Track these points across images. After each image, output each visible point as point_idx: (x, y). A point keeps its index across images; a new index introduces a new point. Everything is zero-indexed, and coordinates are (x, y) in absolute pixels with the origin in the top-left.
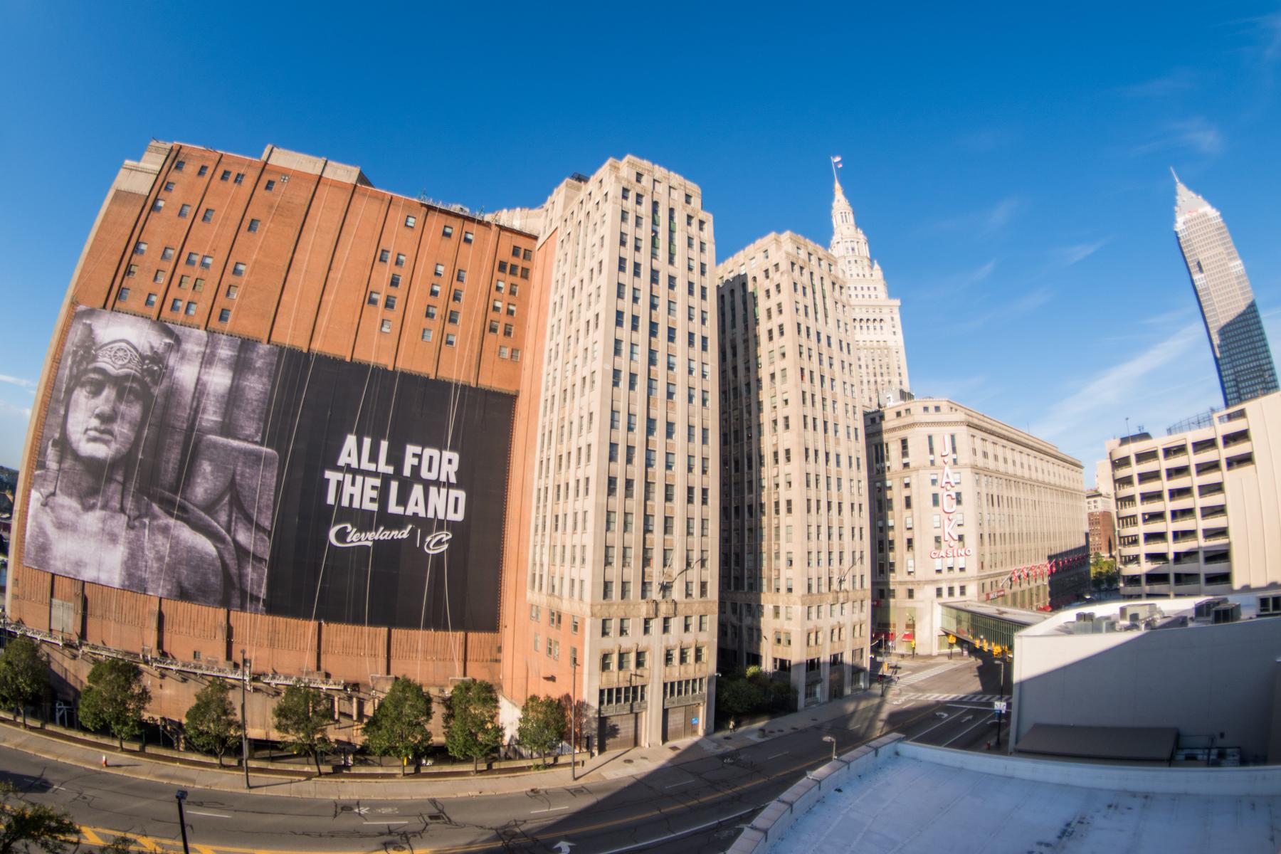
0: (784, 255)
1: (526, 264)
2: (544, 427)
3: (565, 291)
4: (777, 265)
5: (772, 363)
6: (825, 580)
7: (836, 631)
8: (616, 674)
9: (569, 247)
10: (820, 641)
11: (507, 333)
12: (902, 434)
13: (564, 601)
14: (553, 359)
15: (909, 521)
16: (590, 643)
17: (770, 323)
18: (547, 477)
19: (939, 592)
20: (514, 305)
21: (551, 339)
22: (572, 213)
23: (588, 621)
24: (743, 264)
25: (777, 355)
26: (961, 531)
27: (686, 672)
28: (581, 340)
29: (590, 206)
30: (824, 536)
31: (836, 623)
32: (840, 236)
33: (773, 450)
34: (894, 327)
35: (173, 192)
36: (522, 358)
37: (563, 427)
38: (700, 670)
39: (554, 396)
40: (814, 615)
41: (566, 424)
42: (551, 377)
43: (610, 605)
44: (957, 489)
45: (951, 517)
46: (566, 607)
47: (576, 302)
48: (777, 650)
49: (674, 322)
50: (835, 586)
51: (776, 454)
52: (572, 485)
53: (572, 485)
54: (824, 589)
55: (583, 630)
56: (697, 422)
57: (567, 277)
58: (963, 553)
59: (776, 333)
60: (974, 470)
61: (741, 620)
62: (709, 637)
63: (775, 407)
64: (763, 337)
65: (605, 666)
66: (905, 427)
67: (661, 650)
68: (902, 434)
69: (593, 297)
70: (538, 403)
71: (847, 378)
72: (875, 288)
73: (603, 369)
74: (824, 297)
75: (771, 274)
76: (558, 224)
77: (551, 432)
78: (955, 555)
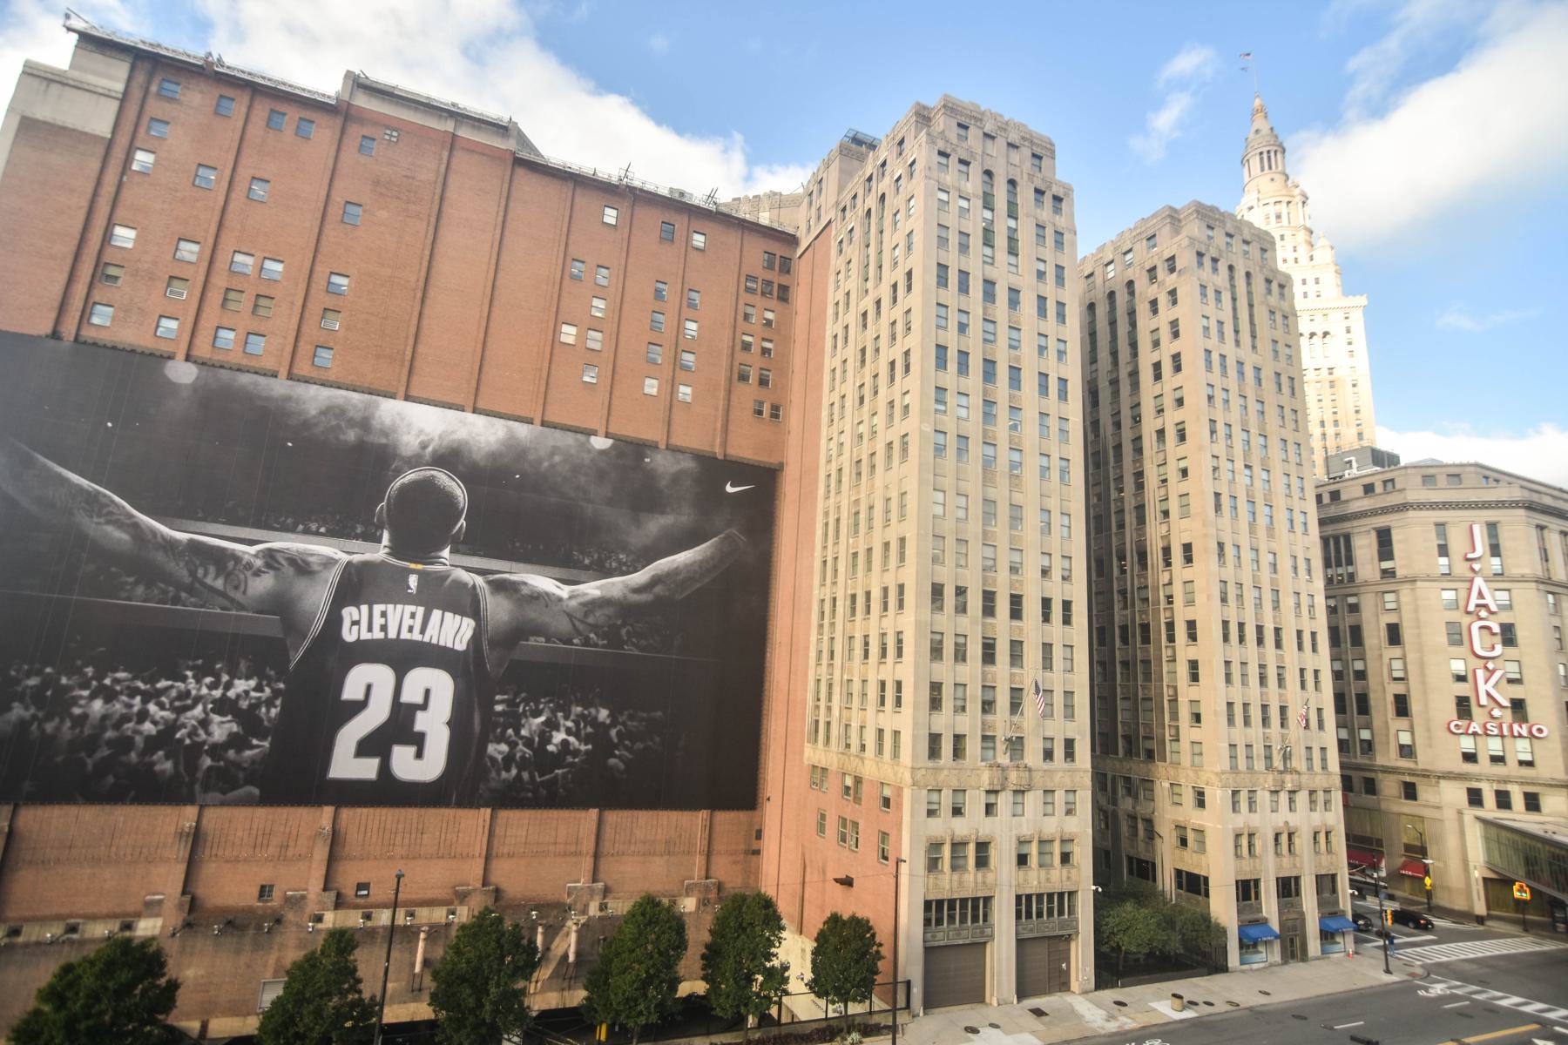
0: (1186, 242)
1: (784, 280)
2: (826, 514)
3: (852, 318)
4: (1172, 259)
5: (1160, 411)
6: (1258, 750)
7: (1285, 839)
8: (947, 877)
9: (852, 251)
10: (1258, 849)
11: (763, 382)
12: (1381, 521)
13: (866, 762)
14: (836, 417)
15: (1397, 665)
16: (912, 823)
17: (1157, 352)
18: (834, 583)
19: (1475, 798)
20: (771, 341)
21: (832, 389)
22: (855, 197)
23: (907, 793)
24: (1112, 262)
25: (1168, 402)
26: (1517, 692)
27: (1048, 880)
28: (882, 390)
29: (885, 185)
30: (1254, 679)
31: (1281, 824)
32: (1255, 195)
33: (1161, 545)
34: (1350, 343)
35: (699, 957)
36: (784, 418)
37: (857, 513)
38: (1068, 878)
39: (840, 470)
40: (1244, 805)
41: (863, 508)
42: (833, 444)
43: (938, 770)
44: (1506, 618)
45: (1490, 665)
46: (870, 769)
47: (871, 333)
48: (1182, 859)
49: (1018, 359)
50: (1277, 762)
51: (1167, 551)
52: (876, 594)
53: (876, 594)
54: (1259, 765)
55: (899, 806)
56: (1053, 504)
57: (853, 296)
58: (1524, 732)
59: (1167, 368)
60: (1542, 587)
61: (1114, 802)
62: (1081, 827)
63: (1165, 481)
64: (1146, 375)
65: (933, 864)
66: (1385, 511)
67: (1010, 841)
68: (1381, 521)
69: (900, 327)
70: (816, 481)
71: (1288, 434)
72: (1317, 281)
73: (921, 432)
74: (1251, 306)
75: (1161, 273)
76: (832, 215)
77: (838, 520)
78: (1506, 732)
